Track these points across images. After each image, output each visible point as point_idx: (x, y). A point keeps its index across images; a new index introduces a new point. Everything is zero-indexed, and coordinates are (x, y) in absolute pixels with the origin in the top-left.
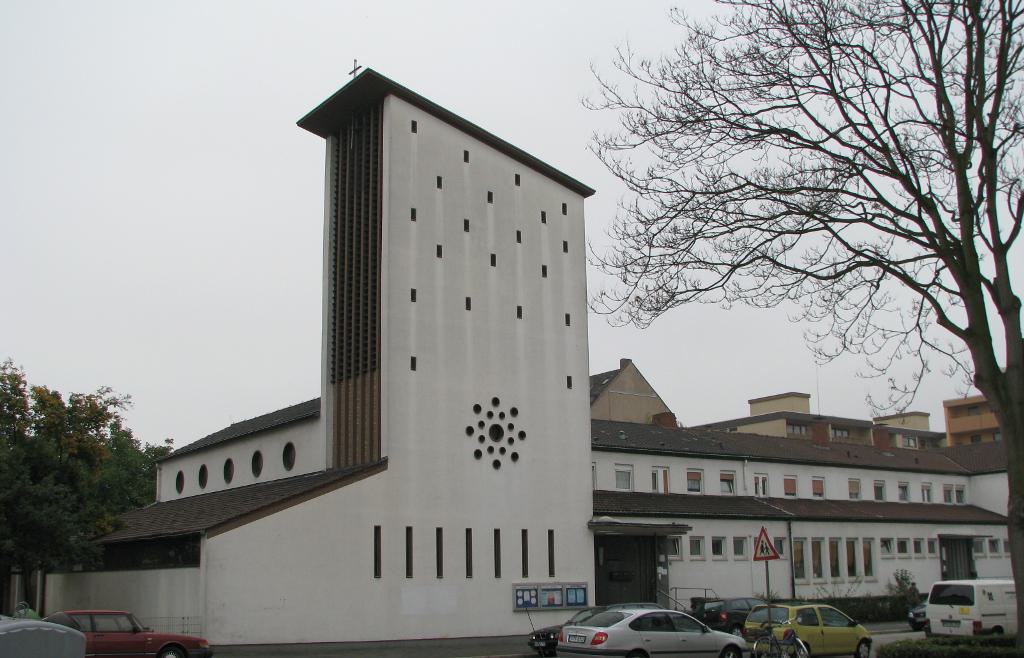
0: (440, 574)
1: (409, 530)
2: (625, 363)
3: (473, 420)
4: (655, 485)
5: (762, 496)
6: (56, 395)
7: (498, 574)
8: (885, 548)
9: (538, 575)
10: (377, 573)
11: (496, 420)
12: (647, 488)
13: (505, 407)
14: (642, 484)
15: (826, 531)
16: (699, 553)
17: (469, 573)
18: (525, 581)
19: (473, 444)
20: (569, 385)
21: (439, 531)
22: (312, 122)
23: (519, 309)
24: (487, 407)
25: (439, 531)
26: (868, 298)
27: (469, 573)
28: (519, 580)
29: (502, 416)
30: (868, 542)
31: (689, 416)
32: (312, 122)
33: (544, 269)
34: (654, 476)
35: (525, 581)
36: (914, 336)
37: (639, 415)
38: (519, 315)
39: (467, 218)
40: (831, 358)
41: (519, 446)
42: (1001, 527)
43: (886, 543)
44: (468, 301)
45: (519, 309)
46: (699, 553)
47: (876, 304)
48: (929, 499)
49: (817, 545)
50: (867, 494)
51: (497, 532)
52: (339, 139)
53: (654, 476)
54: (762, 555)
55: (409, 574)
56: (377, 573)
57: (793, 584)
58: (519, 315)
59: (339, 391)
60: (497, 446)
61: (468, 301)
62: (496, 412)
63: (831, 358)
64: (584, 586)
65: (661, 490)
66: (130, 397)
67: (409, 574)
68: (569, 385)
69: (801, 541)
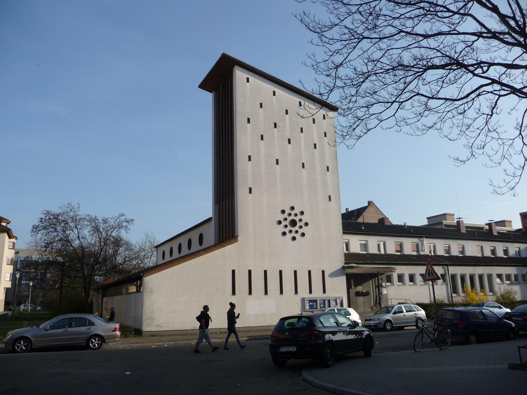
0: (266, 293)
2: (370, 203)
3: (281, 217)
5: (433, 254)
7: (296, 292)
9: (317, 294)
11: (292, 217)
12: (375, 251)
14: (373, 250)
15: (468, 270)
20: (330, 200)
21: (265, 272)
23: (303, 164)
24: (288, 211)
25: (265, 272)
26: (485, 123)
30: (490, 276)
31: (395, 220)
32: (204, 85)
33: (315, 145)
34: (379, 245)
36: (519, 141)
37: (375, 220)
38: (303, 167)
40: (464, 162)
41: (305, 230)
43: (500, 276)
44: (277, 160)
45: (303, 164)
47: (490, 128)
48: (519, 255)
49: (463, 278)
50: (488, 253)
52: (217, 92)
53: (379, 245)
54: (429, 278)
57: (11, 242)
58: (303, 167)
59: (219, 207)
60: (294, 229)
61: (277, 160)
62: (293, 213)
63: (464, 162)
65: (383, 252)
68: (330, 200)
69: (453, 277)
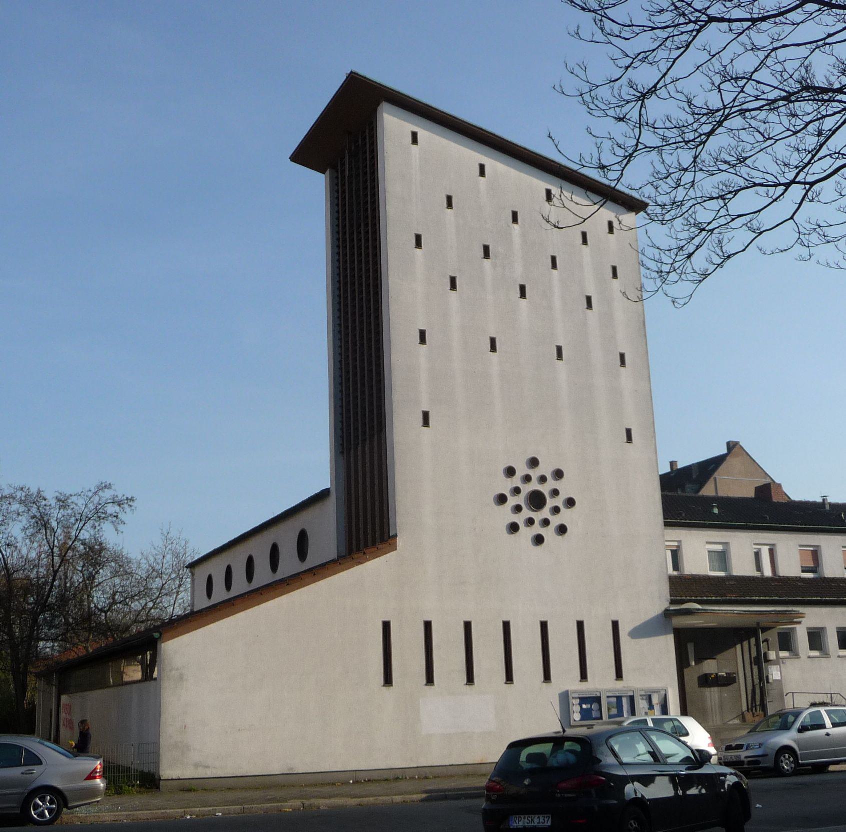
0: (470, 680)
1: (428, 626)
3: (505, 486)
4: (759, 567)
6: (39, 495)
7: (547, 677)
8: (770, 662)
10: (388, 680)
11: (534, 486)
12: (751, 571)
13: (546, 468)
16: (746, 722)
17: (509, 678)
18: (620, 685)
19: (506, 514)
20: (629, 438)
21: (468, 626)
22: (301, 155)
23: (559, 350)
24: (522, 469)
25: (468, 626)
27: (509, 678)
28: (575, 686)
29: (555, 493)
34: (758, 555)
35: (620, 685)
38: (560, 355)
39: (487, 243)
41: (566, 517)
42: (685, 673)
45: (559, 350)
46: (746, 722)
51: (544, 626)
53: (758, 555)
55: (430, 680)
56: (388, 680)
58: (560, 355)
62: (535, 474)
64: (666, 689)
65: (768, 572)
66: (133, 501)
67: (430, 680)
68: (629, 438)
